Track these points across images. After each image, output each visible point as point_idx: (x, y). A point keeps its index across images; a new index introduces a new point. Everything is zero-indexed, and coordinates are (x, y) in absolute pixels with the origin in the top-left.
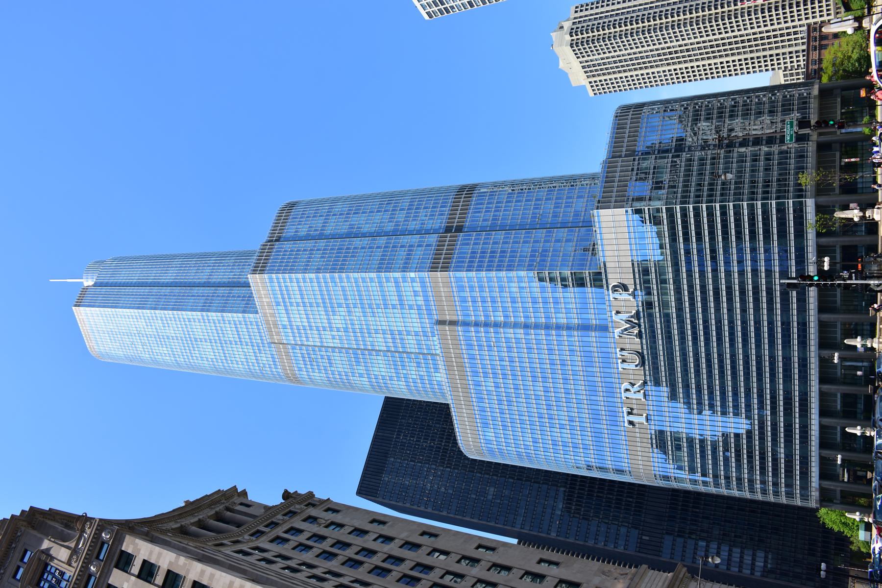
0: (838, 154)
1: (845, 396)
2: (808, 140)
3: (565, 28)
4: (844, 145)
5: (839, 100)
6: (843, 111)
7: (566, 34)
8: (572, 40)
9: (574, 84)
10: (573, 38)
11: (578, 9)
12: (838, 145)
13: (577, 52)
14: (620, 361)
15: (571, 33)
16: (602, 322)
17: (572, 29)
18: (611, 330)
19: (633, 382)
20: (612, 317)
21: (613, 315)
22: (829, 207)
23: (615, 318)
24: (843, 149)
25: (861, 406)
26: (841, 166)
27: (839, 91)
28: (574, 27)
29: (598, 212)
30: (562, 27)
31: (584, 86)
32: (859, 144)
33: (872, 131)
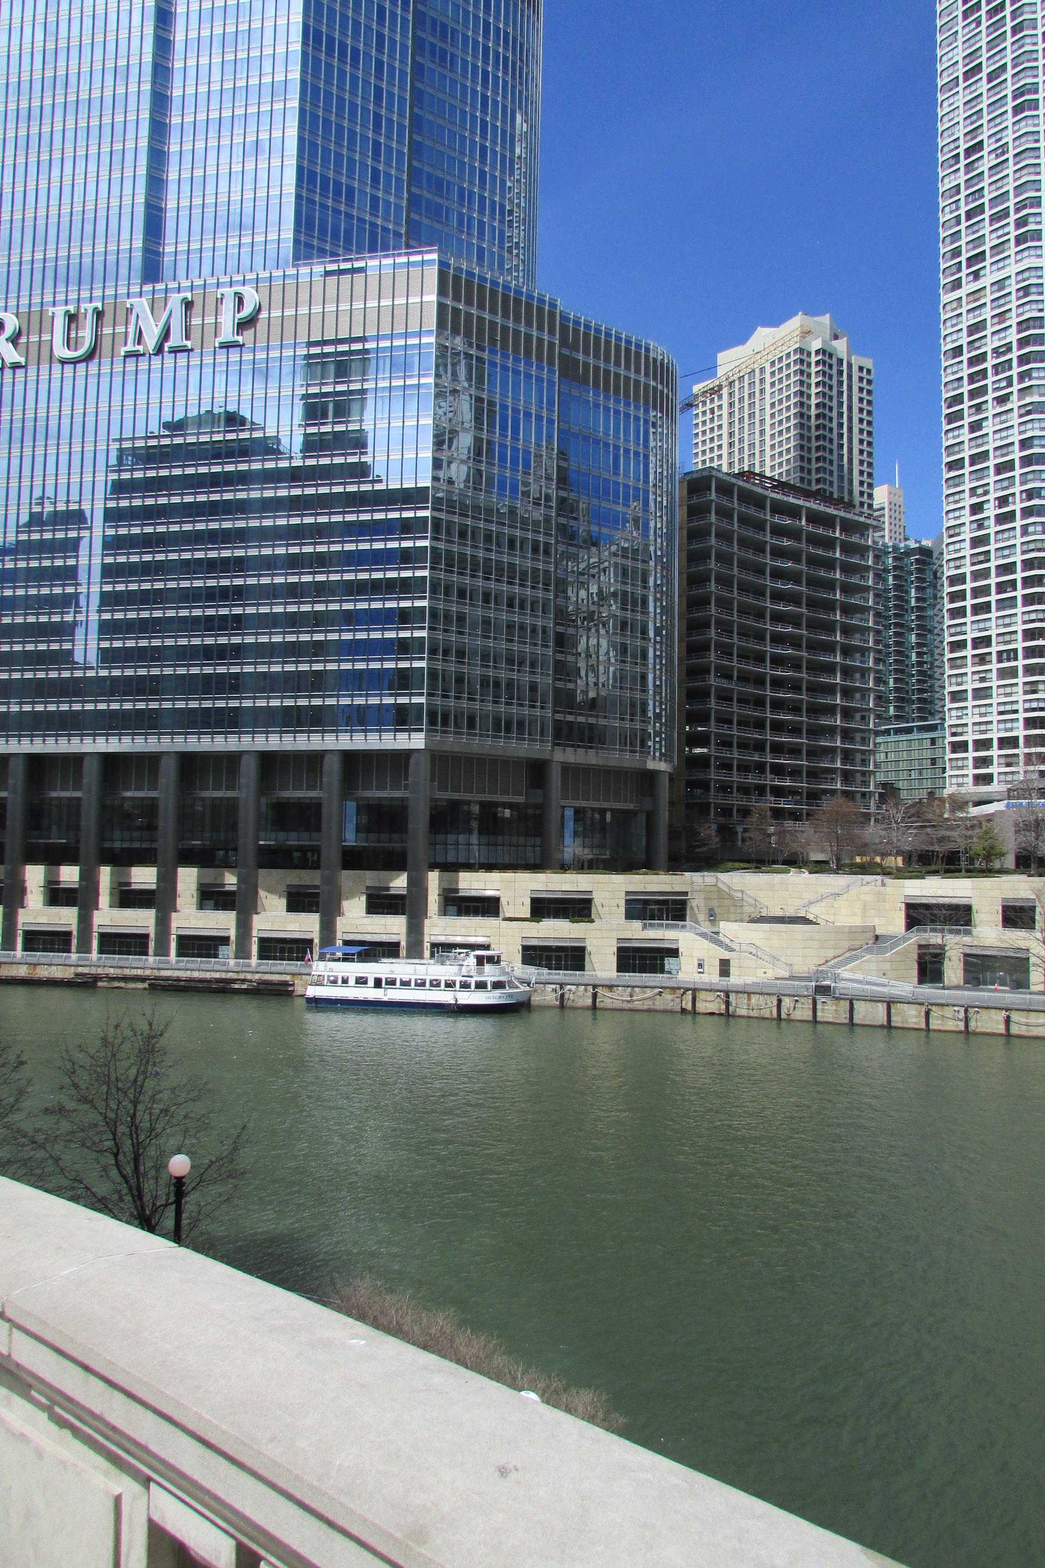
0: (520, 799)
1: (150, 808)
2: (555, 744)
3: (835, 343)
4: (538, 812)
5: (631, 807)
6: (608, 816)
7: (824, 341)
8: (809, 354)
9: (722, 357)
10: (813, 354)
11: (864, 374)
12: (539, 801)
13: (785, 362)
14: (72, 308)
15: (824, 352)
16: (167, 272)
17: (831, 356)
18: (148, 288)
19: (23, 340)
20: (179, 290)
21: (183, 295)
22: (406, 779)
23: (175, 300)
24: (530, 811)
25: (293, 839)
26: (495, 804)
27: (648, 806)
28: (834, 361)
29: (432, 261)
30: (836, 337)
31: (714, 375)
32: (538, 841)
33: (558, 1394)
